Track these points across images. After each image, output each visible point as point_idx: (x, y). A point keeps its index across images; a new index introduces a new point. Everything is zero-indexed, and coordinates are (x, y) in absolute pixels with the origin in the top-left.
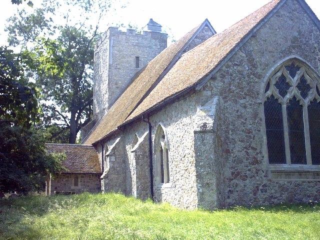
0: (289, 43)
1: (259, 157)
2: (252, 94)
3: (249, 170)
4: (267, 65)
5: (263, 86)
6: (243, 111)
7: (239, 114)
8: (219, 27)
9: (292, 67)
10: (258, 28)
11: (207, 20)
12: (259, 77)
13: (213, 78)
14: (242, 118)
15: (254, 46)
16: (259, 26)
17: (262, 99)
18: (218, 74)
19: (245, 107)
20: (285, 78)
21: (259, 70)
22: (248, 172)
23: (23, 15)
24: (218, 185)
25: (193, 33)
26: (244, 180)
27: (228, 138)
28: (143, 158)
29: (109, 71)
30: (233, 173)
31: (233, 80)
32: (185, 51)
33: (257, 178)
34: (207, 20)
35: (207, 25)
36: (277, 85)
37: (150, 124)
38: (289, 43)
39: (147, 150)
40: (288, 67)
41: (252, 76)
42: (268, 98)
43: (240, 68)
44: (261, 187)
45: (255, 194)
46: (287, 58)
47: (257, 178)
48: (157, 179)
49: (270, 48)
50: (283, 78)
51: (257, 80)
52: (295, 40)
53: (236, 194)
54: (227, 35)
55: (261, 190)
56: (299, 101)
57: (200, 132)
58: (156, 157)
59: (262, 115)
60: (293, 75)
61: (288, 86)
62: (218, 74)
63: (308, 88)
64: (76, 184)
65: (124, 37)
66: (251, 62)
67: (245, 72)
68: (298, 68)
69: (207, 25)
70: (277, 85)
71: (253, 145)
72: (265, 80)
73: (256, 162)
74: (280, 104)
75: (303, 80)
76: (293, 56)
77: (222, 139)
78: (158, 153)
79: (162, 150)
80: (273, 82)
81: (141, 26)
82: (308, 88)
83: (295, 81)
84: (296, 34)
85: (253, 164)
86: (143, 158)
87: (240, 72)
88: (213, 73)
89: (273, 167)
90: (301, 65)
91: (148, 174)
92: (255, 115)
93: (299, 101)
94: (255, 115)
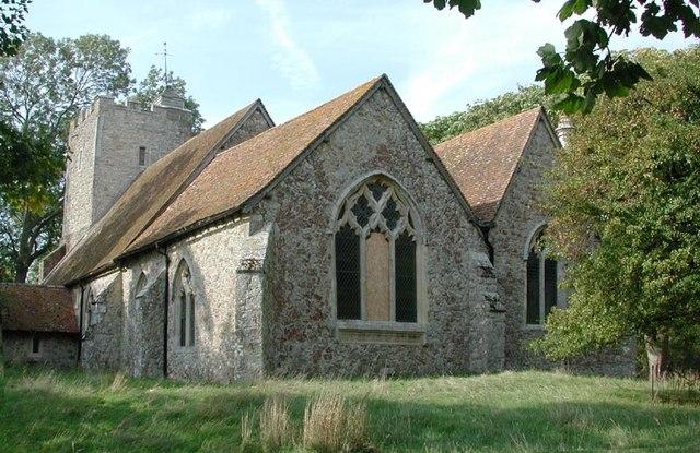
0: (374, 153)
1: (324, 309)
2: (320, 220)
3: (309, 327)
4: (342, 183)
5: (335, 211)
6: (306, 245)
7: (300, 247)
8: (280, 113)
9: (378, 185)
10: (332, 130)
11: (259, 100)
12: (332, 198)
13: (268, 198)
14: (304, 253)
15: (324, 155)
16: (335, 127)
17: (334, 227)
18: (274, 193)
19: (309, 239)
20: (367, 202)
21: (331, 188)
22: (307, 330)
23: (260, 218)
24: (265, 346)
25: (236, 121)
26: (301, 341)
27: (283, 280)
28: (154, 308)
29: (95, 169)
30: (286, 331)
31: (295, 201)
32: (223, 148)
33: (320, 338)
34: (259, 100)
35: (259, 107)
36: (354, 210)
37: (167, 257)
38: (374, 153)
39: (161, 296)
40: (371, 186)
41: (321, 197)
42: (341, 228)
43: (305, 185)
44: (324, 352)
45: (315, 362)
46: (370, 174)
47: (320, 338)
48: (174, 340)
49: (347, 159)
50: (363, 201)
51: (328, 202)
52: (382, 149)
53: (289, 360)
54: (293, 125)
55: (325, 356)
56: (354, 230)
57: (245, 271)
58: (174, 307)
59: (331, 249)
60: (377, 196)
61: (385, 214)
62: (274, 193)
63: (397, 215)
64: (36, 350)
65: (123, 114)
66: (321, 177)
67: (312, 192)
68: (385, 188)
69: (259, 107)
70: (354, 210)
71: (317, 292)
72: (339, 203)
73: (320, 316)
74: (358, 237)
75: (391, 204)
76: (376, 172)
77: (275, 282)
78: (178, 301)
79: (183, 298)
80: (350, 205)
81: (122, 47)
82: (397, 215)
83: (379, 205)
84: (384, 141)
85: (315, 319)
86: (154, 308)
87: (305, 191)
88: (268, 190)
89: (342, 324)
90: (388, 184)
91: (160, 334)
92: (323, 251)
93: (354, 230)
94: (323, 251)
